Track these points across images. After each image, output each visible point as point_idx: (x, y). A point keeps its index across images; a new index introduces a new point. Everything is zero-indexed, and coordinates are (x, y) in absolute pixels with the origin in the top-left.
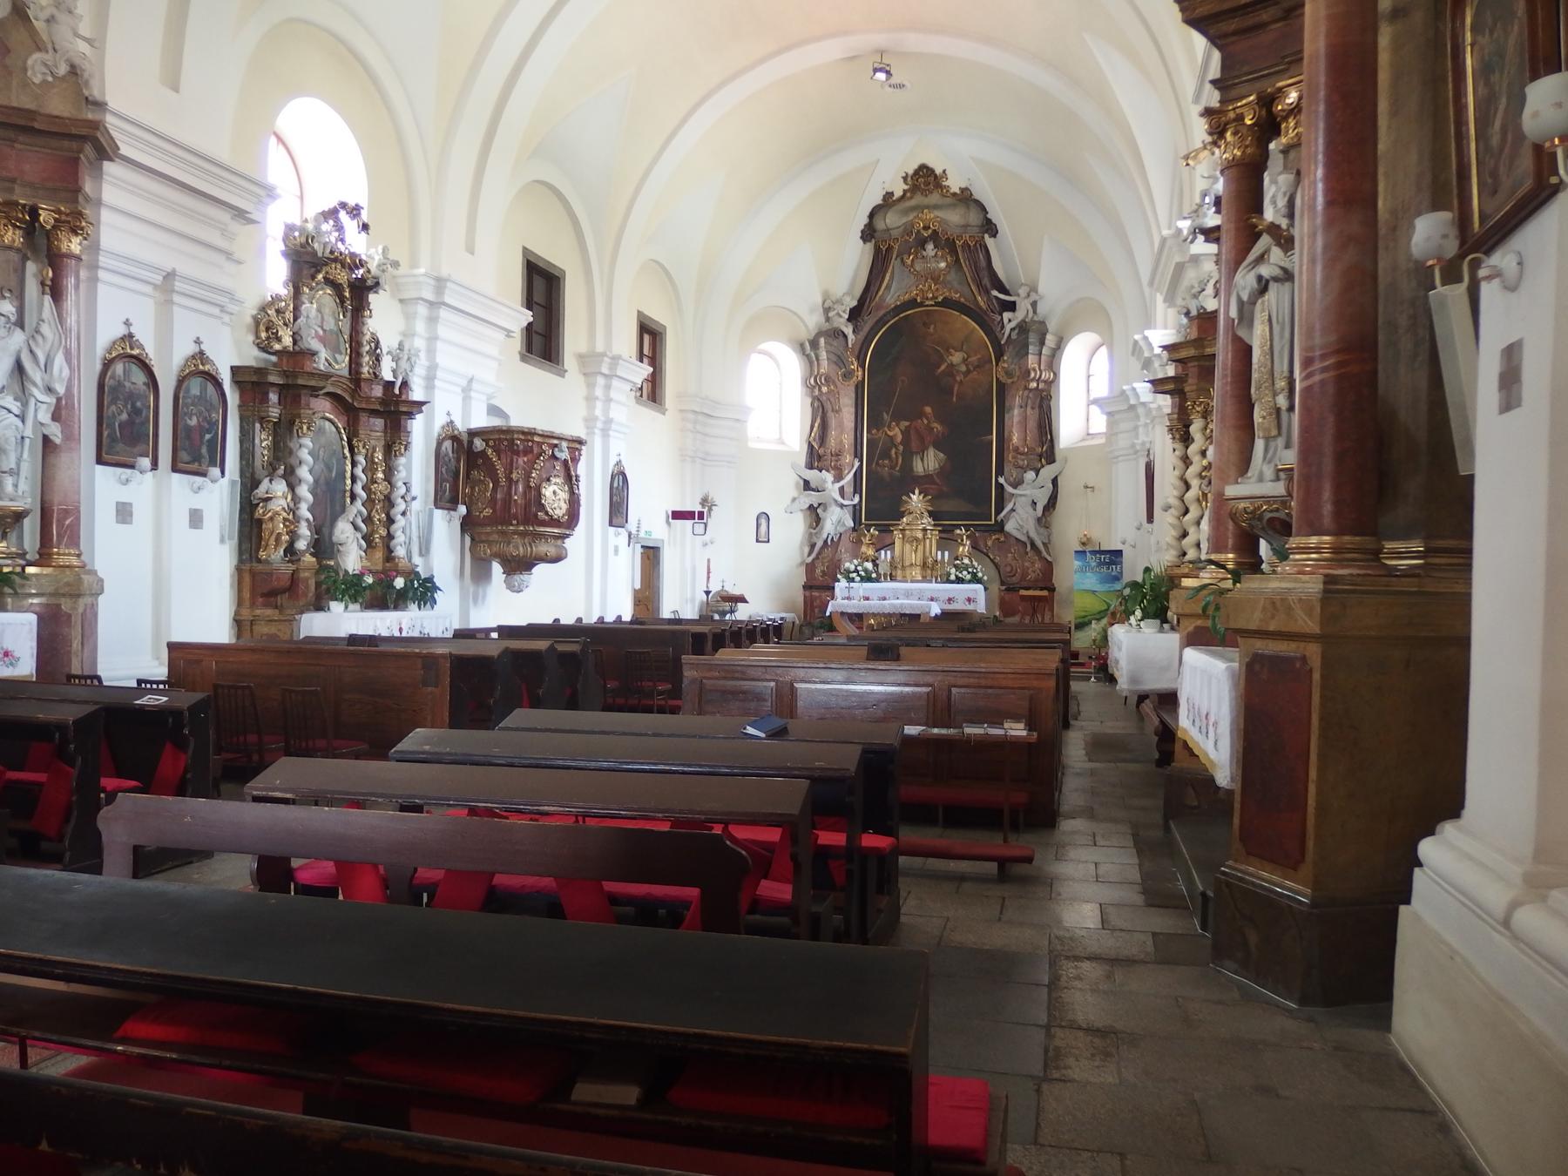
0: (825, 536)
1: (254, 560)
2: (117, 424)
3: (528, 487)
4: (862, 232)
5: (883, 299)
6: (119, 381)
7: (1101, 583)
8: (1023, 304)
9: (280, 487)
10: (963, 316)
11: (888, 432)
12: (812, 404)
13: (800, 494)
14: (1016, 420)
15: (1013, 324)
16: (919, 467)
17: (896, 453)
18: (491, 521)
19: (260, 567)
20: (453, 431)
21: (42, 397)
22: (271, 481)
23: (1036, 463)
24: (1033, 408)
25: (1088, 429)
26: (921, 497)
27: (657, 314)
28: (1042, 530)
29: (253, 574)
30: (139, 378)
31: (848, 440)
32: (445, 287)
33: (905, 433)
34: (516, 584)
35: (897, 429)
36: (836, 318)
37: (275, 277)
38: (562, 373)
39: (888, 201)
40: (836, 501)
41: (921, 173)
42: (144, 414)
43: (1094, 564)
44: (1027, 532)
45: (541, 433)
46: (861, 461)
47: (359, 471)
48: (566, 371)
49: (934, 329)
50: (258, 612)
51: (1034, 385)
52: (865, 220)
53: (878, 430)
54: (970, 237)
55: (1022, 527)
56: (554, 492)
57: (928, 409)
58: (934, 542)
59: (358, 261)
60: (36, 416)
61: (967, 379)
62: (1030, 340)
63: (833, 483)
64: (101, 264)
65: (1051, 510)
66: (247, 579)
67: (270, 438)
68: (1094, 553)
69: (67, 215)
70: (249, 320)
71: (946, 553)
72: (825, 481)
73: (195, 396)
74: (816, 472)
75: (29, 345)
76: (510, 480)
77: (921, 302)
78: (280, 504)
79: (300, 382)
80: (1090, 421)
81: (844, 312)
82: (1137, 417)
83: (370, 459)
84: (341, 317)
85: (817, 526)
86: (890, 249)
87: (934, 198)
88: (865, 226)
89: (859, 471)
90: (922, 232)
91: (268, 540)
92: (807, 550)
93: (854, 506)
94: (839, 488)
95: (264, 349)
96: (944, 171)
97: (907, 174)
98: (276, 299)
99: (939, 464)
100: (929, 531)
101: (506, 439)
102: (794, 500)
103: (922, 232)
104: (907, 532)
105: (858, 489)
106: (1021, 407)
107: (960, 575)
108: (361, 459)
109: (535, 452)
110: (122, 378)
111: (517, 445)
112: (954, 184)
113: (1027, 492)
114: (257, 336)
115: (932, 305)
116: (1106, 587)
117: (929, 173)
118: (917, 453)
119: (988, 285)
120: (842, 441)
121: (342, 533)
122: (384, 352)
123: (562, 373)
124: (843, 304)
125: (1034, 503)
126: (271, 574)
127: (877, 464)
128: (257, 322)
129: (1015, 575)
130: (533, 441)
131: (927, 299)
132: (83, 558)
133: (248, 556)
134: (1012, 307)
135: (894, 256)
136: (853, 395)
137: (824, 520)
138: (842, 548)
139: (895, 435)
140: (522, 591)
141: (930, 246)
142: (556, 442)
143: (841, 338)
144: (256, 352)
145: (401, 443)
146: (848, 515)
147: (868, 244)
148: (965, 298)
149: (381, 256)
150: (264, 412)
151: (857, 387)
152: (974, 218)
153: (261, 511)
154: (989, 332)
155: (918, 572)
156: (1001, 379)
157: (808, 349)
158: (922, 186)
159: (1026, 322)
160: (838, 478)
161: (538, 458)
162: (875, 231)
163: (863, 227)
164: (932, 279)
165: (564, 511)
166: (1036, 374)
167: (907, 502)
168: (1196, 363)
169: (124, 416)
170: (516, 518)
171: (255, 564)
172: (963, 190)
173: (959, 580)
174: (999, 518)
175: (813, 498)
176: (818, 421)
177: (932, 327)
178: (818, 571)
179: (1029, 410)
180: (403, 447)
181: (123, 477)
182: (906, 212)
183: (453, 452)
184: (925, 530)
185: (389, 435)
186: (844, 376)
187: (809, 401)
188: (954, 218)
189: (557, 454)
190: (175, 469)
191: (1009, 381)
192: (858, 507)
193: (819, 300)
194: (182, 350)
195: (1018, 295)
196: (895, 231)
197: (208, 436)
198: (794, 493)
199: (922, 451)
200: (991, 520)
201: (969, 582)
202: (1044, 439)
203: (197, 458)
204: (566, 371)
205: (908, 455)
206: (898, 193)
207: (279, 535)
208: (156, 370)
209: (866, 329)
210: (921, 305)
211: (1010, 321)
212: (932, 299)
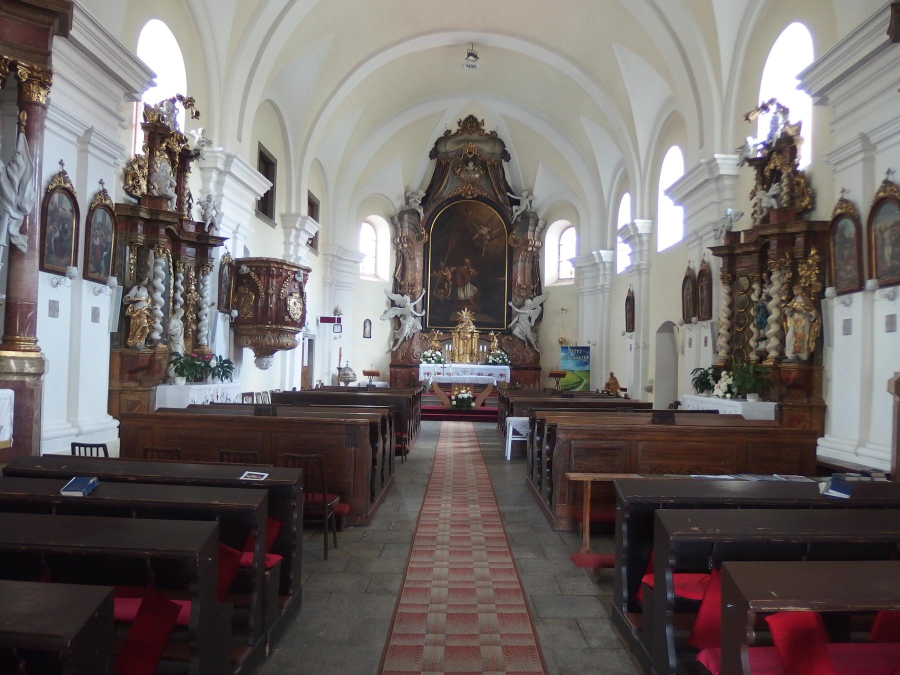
1: (123, 345)
2: (53, 240)
3: (278, 299)
4: (430, 152)
5: (442, 193)
6: (56, 206)
8: (524, 202)
9: (144, 294)
11: (443, 273)
14: (519, 268)
15: (518, 213)
16: (461, 295)
17: (448, 286)
18: (254, 321)
19: (129, 351)
20: (229, 259)
21: (14, 214)
22: (138, 288)
23: (531, 295)
24: (529, 262)
26: (469, 312)
27: (317, 194)
28: (534, 334)
29: (122, 355)
30: (67, 205)
31: (419, 276)
32: (232, 161)
33: (454, 274)
34: (265, 364)
35: (449, 271)
37: (137, 143)
38: (274, 225)
39: (447, 136)
40: (412, 313)
41: (469, 120)
42: (69, 234)
45: (288, 263)
46: (427, 290)
47: (179, 283)
48: (276, 225)
50: (126, 384)
51: (530, 249)
52: (433, 146)
53: (437, 272)
54: (495, 160)
55: (523, 332)
56: (295, 303)
57: (467, 261)
58: (477, 339)
59: (184, 138)
60: (8, 229)
62: (530, 222)
64: (48, 115)
65: (539, 322)
66: (118, 359)
67: (136, 257)
69: (39, 72)
70: (121, 171)
71: (485, 347)
72: (406, 301)
73: (99, 223)
74: (399, 296)
75: (7, 170)
76: (267, 294)
78: (144, 305)
79: (161, 218)
80: (560, 271)
81: (419, 199)
82: (598, 270)
83: (187, 276)
84: (172, 176)
85: (399, 329)
86: (447, 164)
87: (475, 136)
88: (432, 149)
90: (468, 155)
91: (135, 332)
92: (392, 343)
93: (422, 317)
95: (129, 193)
96: (483, 121)
97: (461, 120)
98: (138, 158)
99: (474, 293)
101: (265, 267)
102: (385, 312)
103: (468, 155)
104: (461, 334)
105: (425, 307)
106: (522, 261)
107: (495, 360)
108: (181, 276)
109: (284, 276)
110: (58, 205)
111: (272, 270)
112: (488, 128)
114: (126, 183)
115: (471, 199)
116: (580, 368)
117: (474, 121)
119: (504, 190)
121: (174, 328)
122: (196, 201)
123: (274, 225)
124: (418, 195)
125: (530, 318)
126: (138, 356)
128: (126, 174)
129: (518, 360)
130: (282, 269)
131: (468, 195)
132: (38, 344)
133: (118, 342)
134: (517, 203)
136: (423, 250)
137: (405, 325)
139: (448, 275)
140: (268, 368)
141: (471, 164)
142: (295, 270)
143: (416, 215)
144: (124, 195)
145: (208, 266)
149: (200, 136)
150: (133, 238)
151: (425, 245)
152: (498, 149)
153: (130, 310)
156: (511, 244)
157: (395, 221)
158: (469, 128)
160: (413, 300)
161: (285, 280)
162: (438, 153)
163: (431, 150)
164: (471, 183)
165: (299, 316)
166: (532, 243)
167: (460, 316)
168: (776, 238)
169: (57, 234)
170: (271, 320)
171: (124, 349)
172: (492, 132)
173: (494, 363)
174: (509, 326)
175: (396, 311)
176: (400, 265)
177: (470, 211)
178: (400, 356)
179: (527, 263)
180: (209, 268)
181: (55, 281)
182: (459, 142)
183: (228, 274)
184: (472, 333)
185: (199, 260)
187: (395, 252)
188: (487, 148)
189: (297, 278)
190: (86, 276)
191: (516, 246)
192: (424, 318)
194: (92, 188)
195: (522, 196)
196: (451, 153)
197: (105, 253)
198: (386, 309)
199: (463, 286)
200: (504, 328)
202: (535, 281)
203: (98, 270)
204: (276, 225)
205: (455, 288)
206: (454, 131)
207: (145, 327)
208: (78, 199)
209: (431, 210)
210: (464, 198)
211: (516, 211)
212: (471, 195)
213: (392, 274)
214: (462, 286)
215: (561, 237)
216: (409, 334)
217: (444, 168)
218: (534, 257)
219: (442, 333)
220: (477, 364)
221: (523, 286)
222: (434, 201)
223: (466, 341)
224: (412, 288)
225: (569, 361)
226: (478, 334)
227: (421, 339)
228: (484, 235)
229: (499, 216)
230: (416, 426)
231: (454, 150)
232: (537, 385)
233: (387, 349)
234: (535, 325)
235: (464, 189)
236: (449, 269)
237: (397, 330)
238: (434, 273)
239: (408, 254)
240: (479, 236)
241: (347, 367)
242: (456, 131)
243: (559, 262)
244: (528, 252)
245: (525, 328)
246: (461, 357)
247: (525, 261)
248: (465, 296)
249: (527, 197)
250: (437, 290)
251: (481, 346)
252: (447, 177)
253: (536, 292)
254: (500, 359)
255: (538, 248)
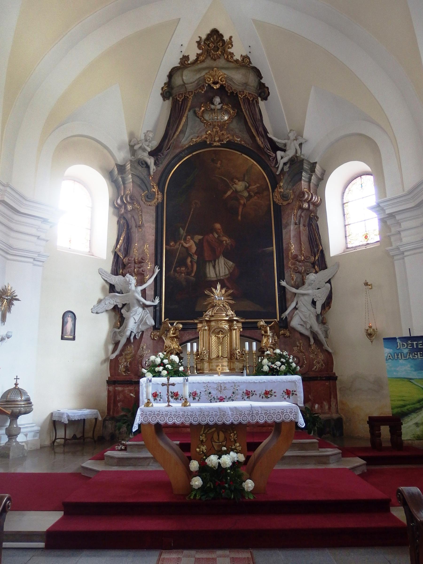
0: (128, 333)
7: (416, 370)
8: (292, 144)
10: (243, 155)
11: (185, 245)
12: (118, 222)
13: (106, 295)
14: (292, 234)
15: (285, 160)
17: (191, 262)
24: (304, 226)
25: (346, 243)
26: (223, 291)
33: (199, 245)
35: (192, 242)
36: (140, 152)
40: (138, 301)
43: (406, 351)
44: (311, 327)
46: (161, 268)
49: (221, 164)
52: (164, 79)
53: (176, 243)
55: (305, 322)
61: (249, 202)
63: (136, 286)
65: (327, 308)
68: (404, 339)
77: (210, 144)
85: (121, 325)
86: (185, 99)
87: (222, 62)
89: (159, 276)
90: (212, 85)
92: (111, 347)
93: (155, 307)
94: (141, 291)
96: (231, 38)
99: (229, 270)
100: (235, 322)
102: (100, 301)
104: (213, 324)
107: (273, 366)
113: (310, 292)
118: (210, 261)
120: (144, 251)
125: (314, 303)
127: (175, 271)
131: (215, 141)
135: (188, 107)
136: (154, 214)
137: (129, 318)
138: (144, 344)
139: (191, 246)
146: (149, 315)
147: (167, 101)
148: (244, 141)
151: (157, 207)
154: (265, 167)
155: (226, 364)
159: (297, 157)
160: (141, 282)
163: (163, 85)
166: (309, 195)
167: (209, 296)
172: (245, 58)
173: (273, 372)
174: (284, 316)
176: (123, 235)
178: (122, 367)
182: (199, 70)
186: (147, 196)
187: (115, 219)
191: (285, 203)
192: (158, 308)
193: (126, 138)
195: (288, 138)
198: (101, 296)
199: (214, 260)
201: (285, 373)
202: (316, 250)
206: (192, 58)
209: (165, 162)
210: (210, 145)
211: (282, 158)
213: (112, 248)
214: (211, 261)
215: (343, 193)
216: (135, 332)
217: (182, 104)
218: (310, 219)
219: (181, 326)
220: (242, 374)
221: (300, 257)
222: (169, 148)
223: (220, 336)
224: (139, 265)
225: (401, 361)
226: (240, 325)
227: (154, 339)
228: (240, 192)
229: (258, 166)
230: (306, 277)
231: (194, 80)
232: (333, 404)
233: (103, 356)
234: (321, 313)
235: (210, 134)
236: (192, 238)
237: (119, 328)
238: (171, 244)
239: (134, 220)
240: (232, 193)
241: (15, 388)
242: (195, 58)
243: (345, 226)
244: (303, 209)
245: (307, 316)
246: (214, 364)
247: (299, 224)
248: (216, 275)
249: (296, 139)
250: (176, 267)
251: (247, 344)
252: (186, 115)
253: (318, 266)
254: (283, 363)
255: (316, 205)
